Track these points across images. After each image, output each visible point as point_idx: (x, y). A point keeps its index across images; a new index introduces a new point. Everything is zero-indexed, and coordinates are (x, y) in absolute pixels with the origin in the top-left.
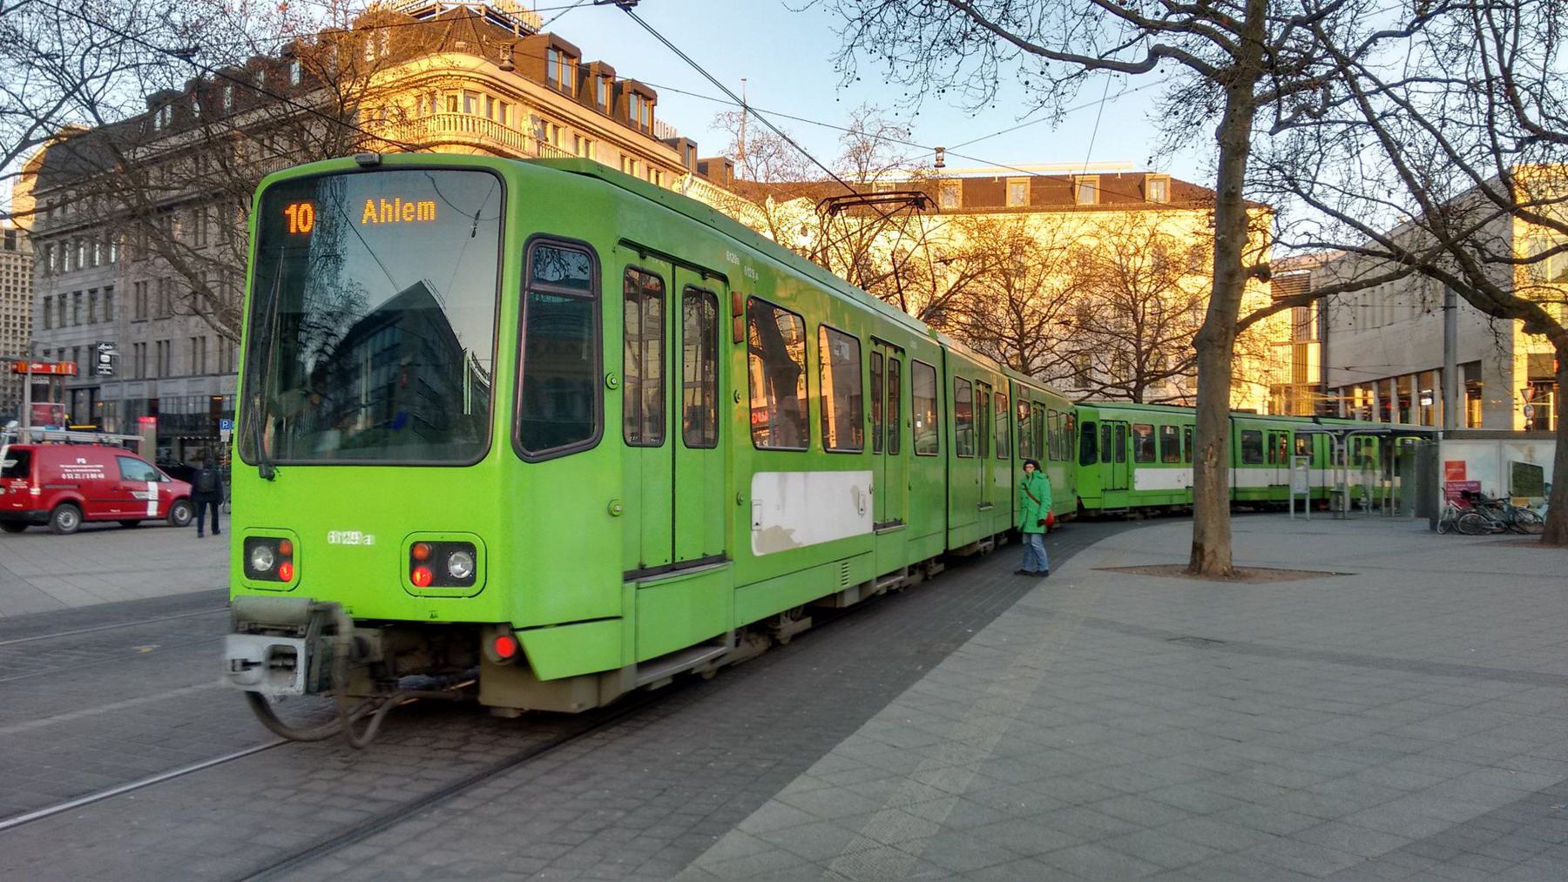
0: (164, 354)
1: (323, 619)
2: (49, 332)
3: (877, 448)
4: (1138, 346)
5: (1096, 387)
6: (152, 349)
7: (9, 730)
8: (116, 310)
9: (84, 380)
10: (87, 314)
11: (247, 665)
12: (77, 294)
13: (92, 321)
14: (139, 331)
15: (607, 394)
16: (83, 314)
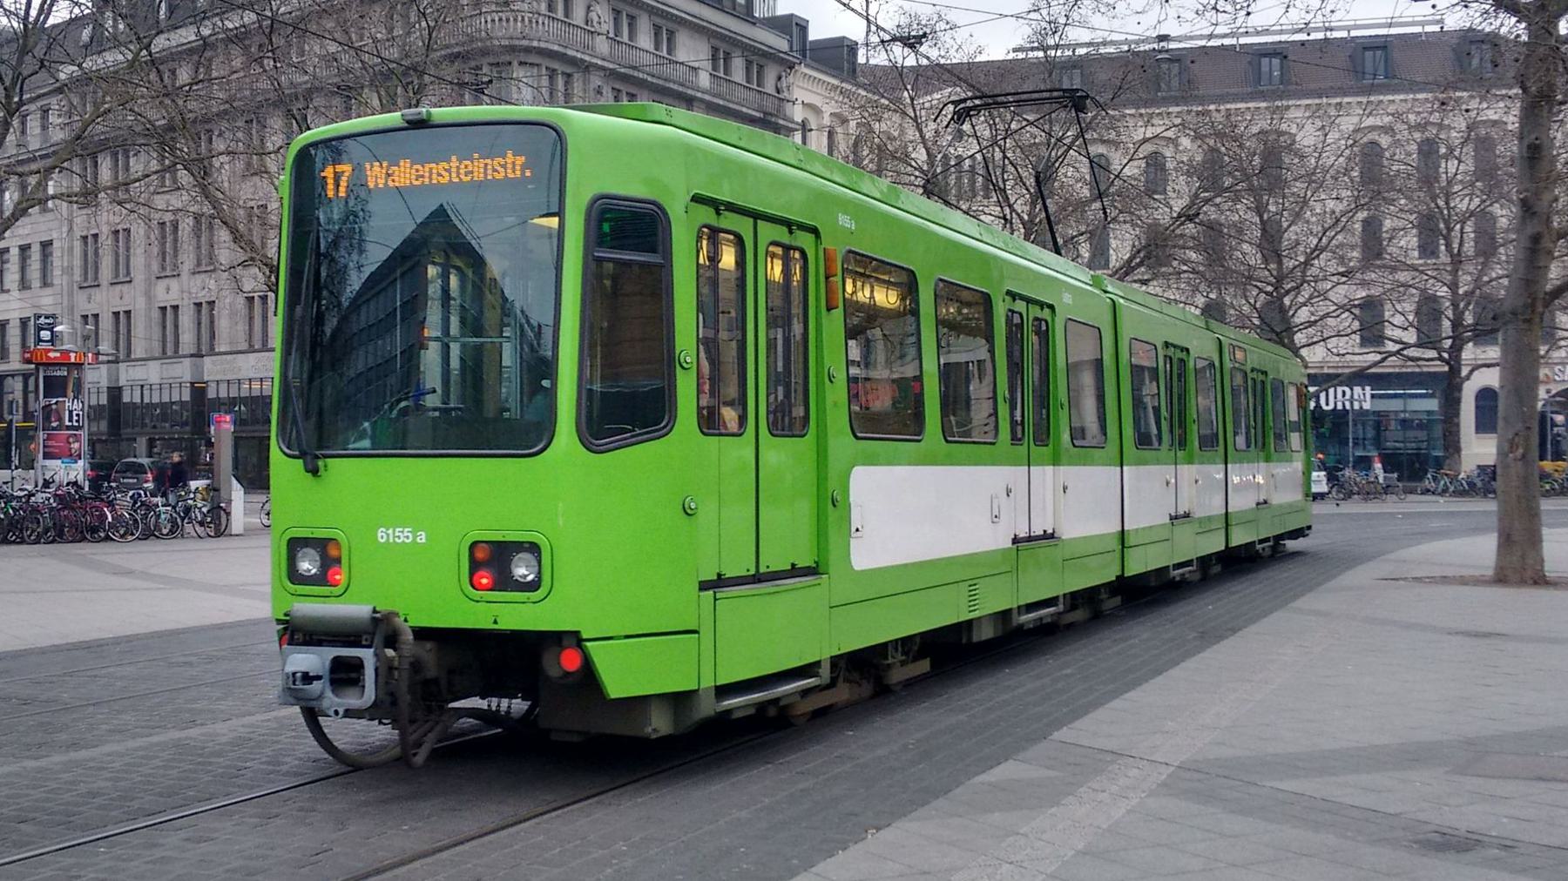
1: (381, 629)
3: (1015, 439)
4: (1453, 286)
5: (1391, 347)
6: (106, 323)
8: (57, 272)
10: (17, 277)
11: (307, 678)
13: (24, 285)
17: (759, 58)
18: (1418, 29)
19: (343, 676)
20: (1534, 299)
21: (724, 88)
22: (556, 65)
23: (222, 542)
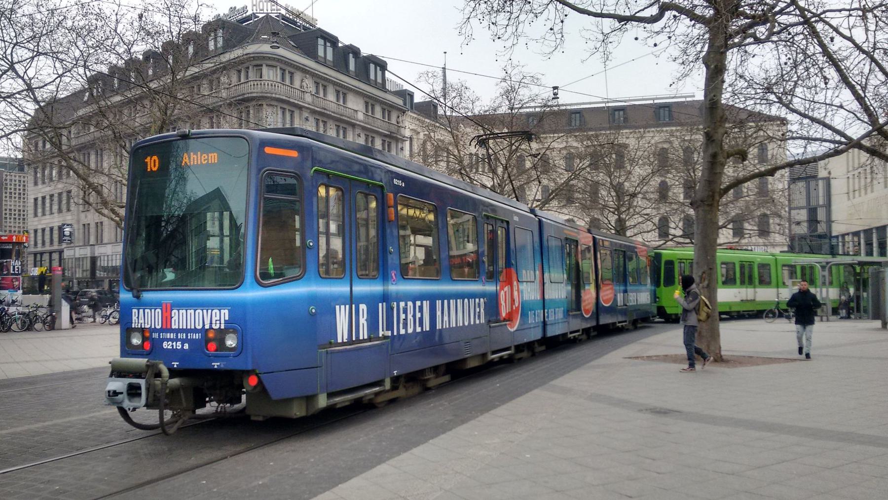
0: (99, 231)
2: (36, 219)
7: (4, 432)
9: (56, 247)
11: (116, 393)
12: (52, 196)
13: (60, 210)
14: (86, 217)
15: (759, 298)
16: (55, 207)
17: (389, 108)
18: (683, 100)
19: (134, 392)
20: (714, 193)
21: (371, 120)
22: (285, 106)
23: (53, 334)
